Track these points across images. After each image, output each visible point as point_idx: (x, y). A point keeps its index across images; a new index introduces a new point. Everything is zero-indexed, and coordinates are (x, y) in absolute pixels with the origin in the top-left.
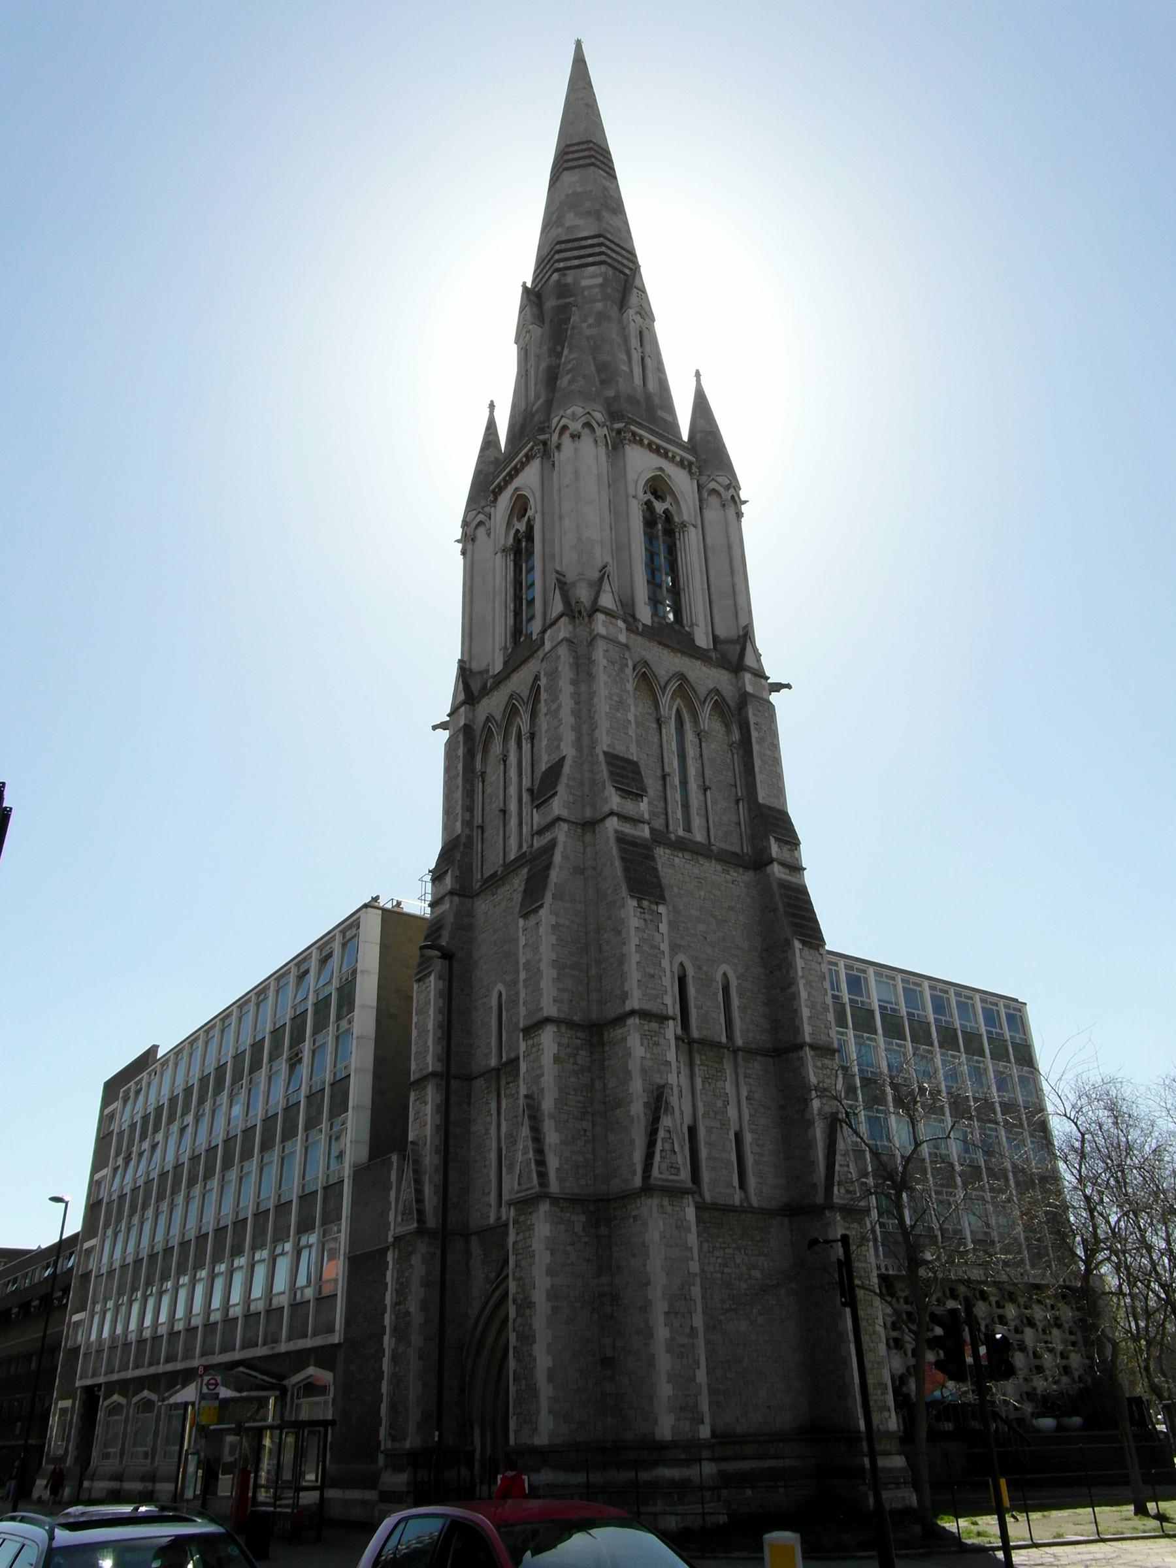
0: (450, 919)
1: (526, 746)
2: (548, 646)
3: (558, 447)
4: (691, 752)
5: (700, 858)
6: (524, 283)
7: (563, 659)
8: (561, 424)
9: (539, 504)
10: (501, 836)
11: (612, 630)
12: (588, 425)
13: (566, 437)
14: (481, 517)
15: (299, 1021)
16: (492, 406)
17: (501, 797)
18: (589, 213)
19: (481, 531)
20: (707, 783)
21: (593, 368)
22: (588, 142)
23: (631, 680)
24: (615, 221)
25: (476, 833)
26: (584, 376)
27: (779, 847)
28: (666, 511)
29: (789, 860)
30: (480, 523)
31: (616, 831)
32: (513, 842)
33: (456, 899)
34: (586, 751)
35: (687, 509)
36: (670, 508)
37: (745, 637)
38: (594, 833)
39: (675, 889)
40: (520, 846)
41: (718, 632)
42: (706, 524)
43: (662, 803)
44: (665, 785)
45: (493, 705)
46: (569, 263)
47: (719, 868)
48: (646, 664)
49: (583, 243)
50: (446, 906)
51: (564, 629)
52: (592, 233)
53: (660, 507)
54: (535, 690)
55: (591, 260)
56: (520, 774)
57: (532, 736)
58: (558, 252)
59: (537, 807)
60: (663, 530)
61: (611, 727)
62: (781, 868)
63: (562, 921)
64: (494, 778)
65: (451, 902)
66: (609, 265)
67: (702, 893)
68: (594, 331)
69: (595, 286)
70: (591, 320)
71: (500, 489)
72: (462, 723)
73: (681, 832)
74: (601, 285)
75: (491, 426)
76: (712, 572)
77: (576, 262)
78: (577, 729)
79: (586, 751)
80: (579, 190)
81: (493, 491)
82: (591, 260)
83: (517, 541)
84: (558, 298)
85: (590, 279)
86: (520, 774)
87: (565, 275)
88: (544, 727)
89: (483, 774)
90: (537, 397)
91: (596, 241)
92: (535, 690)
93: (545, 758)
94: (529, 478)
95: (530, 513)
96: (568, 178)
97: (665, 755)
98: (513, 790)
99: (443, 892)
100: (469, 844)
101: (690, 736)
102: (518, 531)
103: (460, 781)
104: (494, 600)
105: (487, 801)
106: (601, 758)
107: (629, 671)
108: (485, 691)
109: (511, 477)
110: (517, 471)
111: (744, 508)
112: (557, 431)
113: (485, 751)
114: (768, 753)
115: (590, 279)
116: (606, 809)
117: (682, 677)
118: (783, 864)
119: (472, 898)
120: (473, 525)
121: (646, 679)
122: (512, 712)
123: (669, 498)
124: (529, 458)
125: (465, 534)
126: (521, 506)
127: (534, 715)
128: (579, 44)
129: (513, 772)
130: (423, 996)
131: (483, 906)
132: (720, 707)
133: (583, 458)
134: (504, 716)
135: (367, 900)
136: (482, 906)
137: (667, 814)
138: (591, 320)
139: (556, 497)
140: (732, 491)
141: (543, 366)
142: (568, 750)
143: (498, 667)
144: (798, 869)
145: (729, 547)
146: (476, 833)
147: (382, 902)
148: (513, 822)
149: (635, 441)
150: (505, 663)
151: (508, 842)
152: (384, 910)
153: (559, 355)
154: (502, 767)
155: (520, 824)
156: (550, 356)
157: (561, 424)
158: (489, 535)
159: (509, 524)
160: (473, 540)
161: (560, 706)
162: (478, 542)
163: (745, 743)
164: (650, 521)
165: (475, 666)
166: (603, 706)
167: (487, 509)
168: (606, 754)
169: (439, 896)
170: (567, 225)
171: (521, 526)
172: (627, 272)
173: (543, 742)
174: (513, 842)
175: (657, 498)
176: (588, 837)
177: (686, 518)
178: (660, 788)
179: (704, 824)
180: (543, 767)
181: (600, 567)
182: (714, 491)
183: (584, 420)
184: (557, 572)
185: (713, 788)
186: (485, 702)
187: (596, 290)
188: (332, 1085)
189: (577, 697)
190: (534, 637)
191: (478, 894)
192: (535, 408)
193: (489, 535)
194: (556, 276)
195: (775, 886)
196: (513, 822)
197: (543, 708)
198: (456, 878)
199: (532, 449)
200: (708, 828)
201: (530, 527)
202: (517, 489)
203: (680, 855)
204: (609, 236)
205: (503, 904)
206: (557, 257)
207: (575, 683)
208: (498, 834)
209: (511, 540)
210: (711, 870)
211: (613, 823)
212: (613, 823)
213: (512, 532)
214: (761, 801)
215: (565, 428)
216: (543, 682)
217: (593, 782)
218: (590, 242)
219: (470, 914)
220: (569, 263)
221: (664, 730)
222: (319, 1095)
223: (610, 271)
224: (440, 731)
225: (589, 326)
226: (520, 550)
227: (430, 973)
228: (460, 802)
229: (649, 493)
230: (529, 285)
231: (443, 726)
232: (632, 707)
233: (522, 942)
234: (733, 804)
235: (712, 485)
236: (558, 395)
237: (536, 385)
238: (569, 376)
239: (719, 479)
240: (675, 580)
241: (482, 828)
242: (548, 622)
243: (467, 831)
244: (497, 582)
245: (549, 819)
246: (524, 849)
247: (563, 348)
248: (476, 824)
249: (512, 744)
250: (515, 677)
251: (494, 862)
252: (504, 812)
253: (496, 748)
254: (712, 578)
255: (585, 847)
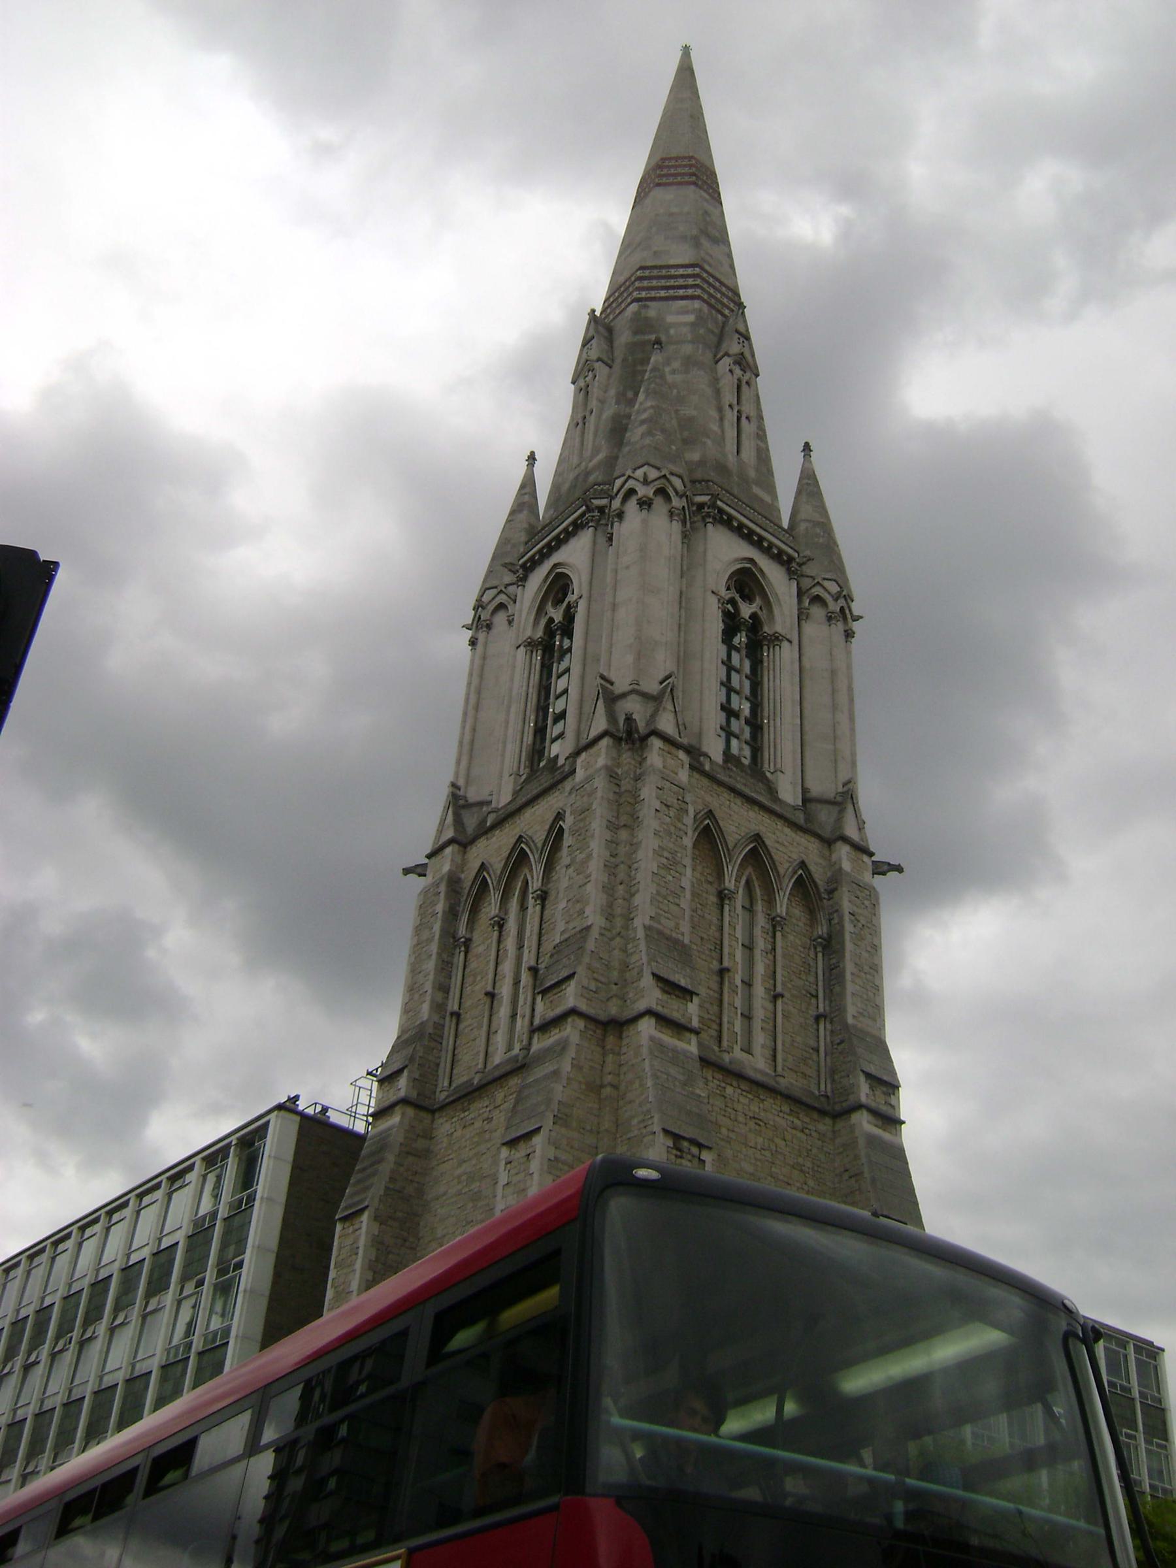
0: (398, 1138)
1: (533, 908)
2: (580, 774)
3: (620, 515)
4: (761, 944)
5: (761, 1091)
6: (593, 311)
7: (599, 794)
8: (627, 486)
9: (585, 586)
10: (485, 1028)
11: (671, 762)
12: (661, 492)
13: (632, 504)
14: (502, 598)
15: (163, 1258)
16: (532, 458)
17: (491, 976)
18: (684, 238)
19: (501, 618)
20: (779, 989)
21: (674, 422)
22: (691, 158)
23: (690, 833)
24: (717, 251)
25: (449, 1024)
26: (663, 431)
27: (872, 1088)
28: (754, 616)
29: (884, 1108)
30: (502, 606)
31: (652, 1039)
32: (500, 1039)
33: (410, 1111)
34: (619, 922)
35: (783, 618)
36: (759, 613)
37: (846, 798)
38: (620, 1038)
39: (724, 1131)
40: (510, 1048)
41: (809, 784)
42: (805, 641)
43: (716, 1008)
44: (721, 983)
45: (493, 851)
46: (653, 294)
47: (786, 1108)
48: (710, 814)
49: (673, 272)
50: (395, 1119)
51: (602, 755)
52: (687, 262)
53: (746, 610)
54: (556, 835)
55: (681, 292)
56: (520, 947)
57: (543, 897)
58: (640, 279)
59: (544, 992)
60: (748, 637)
61: (658, 893)
62: (871, 1118)
63: (564, 1156)
64: (481, 949)
65: (403, 1114)
66: (704, 301)
67: (760, 1140)
68: (678, 378)
69: (685, 324)
70: (676, 365)
71: (529, 568)
72: (446, 868)
73: (738, 1053)
74: (693, 324)
75: (528, 484)
76: (806, 704)
77: (663, 293)
78: (608, 890)
79: (619, 922)
80: (675, 210)
81: (523, 566)
82: (681, 292)
83: (550, 632)
84: (635, 333)
85: (679, 317)
86: (520, 947)
87: (646, 307)
88: (564, 883)
89: (468, 943)
90: (596, 451)
91: (690, 271)
92: (556, 835)
93: (561, 926)
94: (575, 555)
95: (571, 598)
96: (658, 194)
97: (726, 942)
98: (507, 967)
99: (393, 1098)
100: (437, 1037)
101: (761, 921)
102: (551, 620)
103: (434, 947)
104: (509, 707)
105: (469, 980)
106: (641, 933)
107: (689, 820)
108: (485, 831)
109: (551, 549)
110: (560, 542)
111: (856, 626)
112: (621, 495)
113: (475, 910)
114: (865, 954)
115: (679, 317)
116: (642, 1006)
117: (758, 838)
118: (875, 1113)
119: (433, 1112)
120: (491, 607)
121: (709, 836)
122: (518, 859)
123: (758, 601)
124: (577, 527)
125: (477, 619)
126: (559, 586)
127: (549, 867)
128: (686, 50)
129: (510, 943)
130: (349, 1241)
131: (447, 1126)
132: (804, 885)
133: (647, 534)
134: (506, 864)
135: (283, 1099)
136: (444, 1126)
137: (720, 1025)
138: (676, 365)
139: (609, 579)
140: (841, 602)
141: (608, 413)
142: (593, 917)
143: (504, 798)
144: (893, 1122)
145: (833, 673)
146: (449, 1025)
147: (301, 1105)
148: (504, 1011)
149: (722, 522)
150: (516, 793)
151: (490, 1041)
152: (302, 1115)
153: (631, 402)
154: (496, 933)
155: (514, 1016)
156: (618, 403)
157: (627, 486)
158: (510, 622)
159: (541, 610)
160: (489, 627)
161: (590, 856)
162: (494, 631)
163: (830, 945)
164: (732, 623)
165: (473, 795)
166: (647, 862)
167: (512, 589)
168: (647, 928)
169: (387, 1103)
170: (656, 249)
171: (557, 615)
172: (727, 312)
173: (559, 906)
174: (500, 1039)
175: (743, 597)
176: (611, 1040)
177: (779, 628)
178: (715, 986)
179: (770, 1043)
180: (555, 937)
181: (661, 677)
182: (817, 599)
183: (658, 484)
184: (602, 677)
185: (787, 995)
186: (482, 843)
187: (685, 330)
188: (200, 1354)
189: (612, 844)
190: (561, 761)
191: (442, 1108)
192: (591, 465)
193: (510, 622)
194: (634, 307)
195: (862, 1142)
196: (504, 1011)
197: (564, 856)
198: (414, 1081)
199: (583, 514)
200: (775, 1050)
201: (569, 617)
202: (556, 566)
203: (735, 1083)
204: (707, 267)
205: (478, 1124)
206: (637, 284)
207: (613, 827)
208: (480, 1026)
209: (540, 633)
210: (772, 1111)
211: (647, 1027)
212: (647, 1027)
213: (543, 622)
214: (850, 1021)
215: (632, 492)
216: (567, 823)
217: (625, 967)
218: (681, 271)
219: (428, 1135)
220: (653, 294)
221: (727, 908)
222: (180, 1367)
223: (705, 308)
224: (412, 877)
225: (673, 372)
226: (550, 646)
227: (362, 1210)
228: (431, 977)
229: (733, 590)
230: (598, 313)
231: (419, 870)
232: (689, 871)
233: (503, 1178)
234: (811, 1021)
235: (817, 591)
236: (626, 449)
237: (595, 434)
238: (644, 427)
239: (826, 583)
240: (756, 707)
241: (457, 1016)
242: (584, 742)
243: (436, 1018)
244: (516, 684)
245: (559, 1011)
246: (516, 1051)
247: (636, 394)
248: (449, 1009)
249: (514, 904)
250: (528, 814)
251: (469, 1068)
252: (491, 996)
253: (491, 908)
254: (806, 713)
255: (604, 1055)
